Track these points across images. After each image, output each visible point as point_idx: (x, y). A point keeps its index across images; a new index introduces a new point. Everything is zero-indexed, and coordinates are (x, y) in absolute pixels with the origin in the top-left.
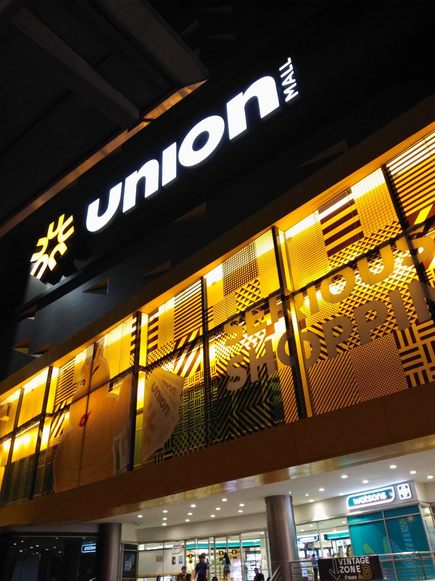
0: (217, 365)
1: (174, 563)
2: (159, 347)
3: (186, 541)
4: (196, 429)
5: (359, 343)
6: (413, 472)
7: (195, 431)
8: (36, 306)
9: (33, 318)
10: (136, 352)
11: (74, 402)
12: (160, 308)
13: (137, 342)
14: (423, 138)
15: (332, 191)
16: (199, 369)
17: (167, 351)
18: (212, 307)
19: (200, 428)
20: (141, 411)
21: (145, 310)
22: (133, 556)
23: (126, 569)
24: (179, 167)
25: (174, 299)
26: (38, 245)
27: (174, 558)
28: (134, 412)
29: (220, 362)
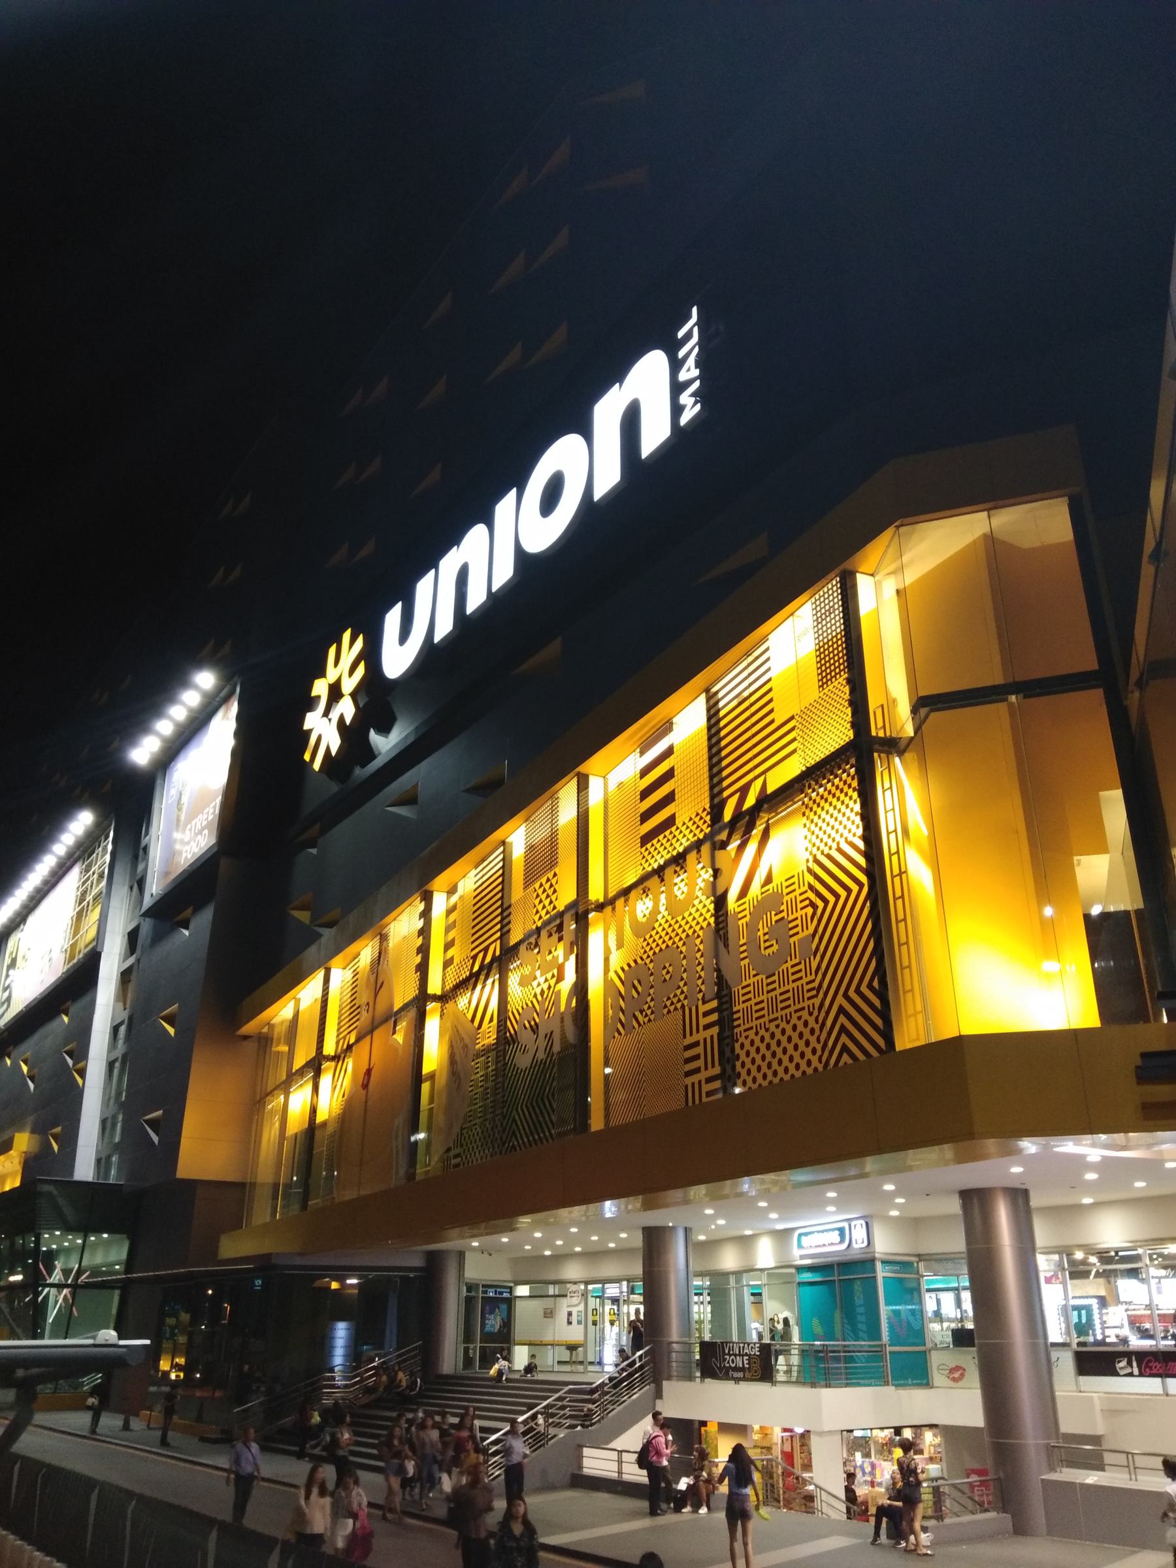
0: (810, 871)
1: (570, 1323)
2: (679, 822)
3: (587, 1283)
4: (795, 1016)
5: (665, 1011)
6: (623, 1235)
7: (794, 1021)
8: (317, 827)
9: (314, 851)
10: (423, 969)
11: (358, 1040)
12: (460, 885)
13: (424, 950)
14: (748, 654)
15: (644, 725)
16: (491, 1020)
17: (677, 845)
18: (792, 718)
19: (805, 1014)
20: (432, 1076)
21: (440, 884)
22: (504, 1307)
23: (488, 1329)
24: (520, 552)
25: (474, 872)
26: (313, 694)
27: (570, 1314)
28: (417, 1077)
29: (817, 861)
